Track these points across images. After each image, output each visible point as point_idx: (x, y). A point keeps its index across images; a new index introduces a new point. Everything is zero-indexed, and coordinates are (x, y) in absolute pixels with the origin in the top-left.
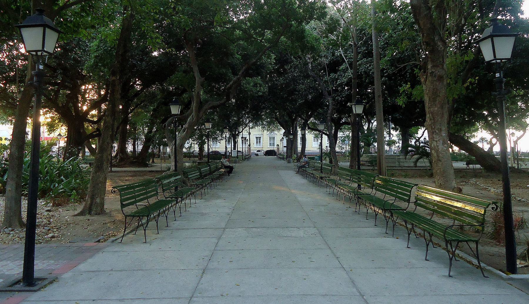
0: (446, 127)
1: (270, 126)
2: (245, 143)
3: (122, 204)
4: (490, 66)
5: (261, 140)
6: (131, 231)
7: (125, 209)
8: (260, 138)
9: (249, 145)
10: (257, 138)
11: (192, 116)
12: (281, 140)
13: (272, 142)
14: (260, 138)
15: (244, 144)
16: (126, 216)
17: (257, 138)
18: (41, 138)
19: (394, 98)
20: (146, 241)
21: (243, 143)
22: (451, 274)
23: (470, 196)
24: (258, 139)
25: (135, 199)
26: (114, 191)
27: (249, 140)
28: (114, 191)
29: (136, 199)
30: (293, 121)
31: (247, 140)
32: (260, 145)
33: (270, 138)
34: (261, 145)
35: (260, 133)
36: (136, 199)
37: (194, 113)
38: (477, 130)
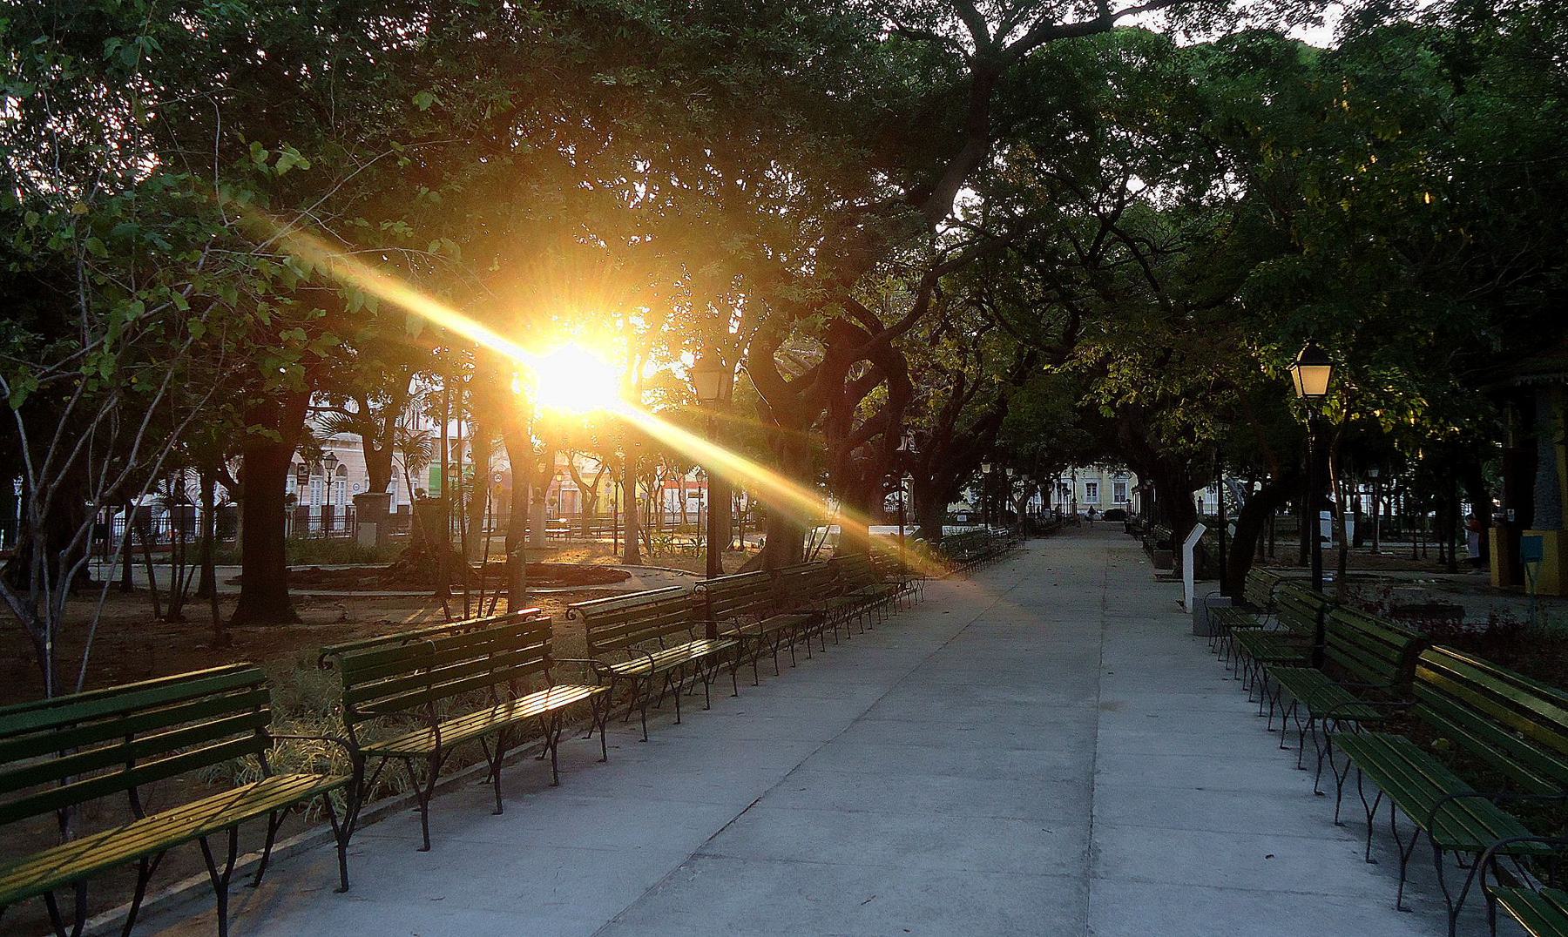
0: (309, 238)
5: (1097, 489)
8: (1096, 485)
9: (1074, 500)
10: (1088, 485)
14: (1096, 485)
17: (1088, 485)
19: (1335, 188)
20: (679, 719)
23: (1442, 653)
24: (1091, 487)
26: (572, 615)
28: (572, 615)
29: (434, 687)
30: (5, 400)
32: (1095, 500)
34: (1098, 499)
35: (1096, 475)
36: (434, 687)
38: (299, 281)
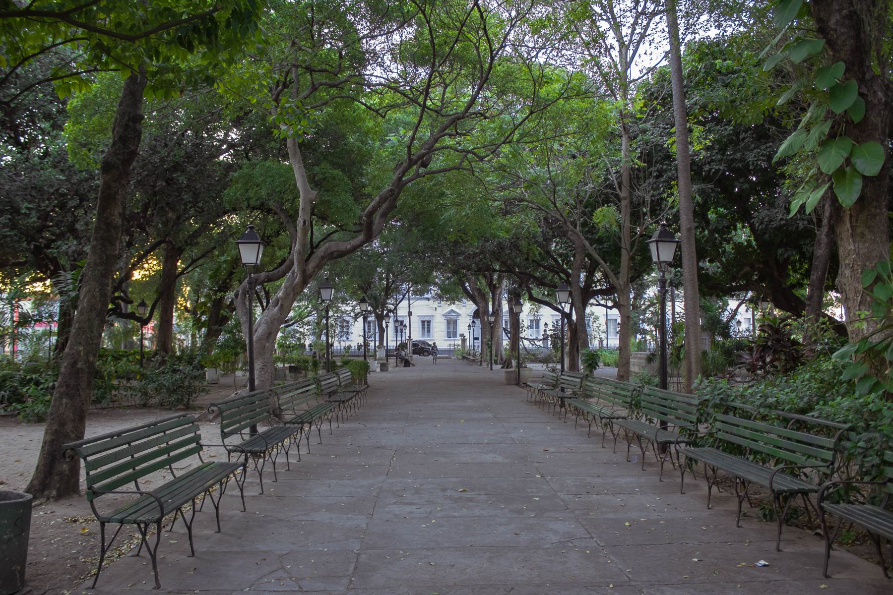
1: (448, 294)
2: (402, 332)
3: (222, 432)
4: (735, 258)
6: (563, 328)
7: (227, 441)
11: (293, 273)
12: (469, 325)
13: (452, 330)
15: (399, 334)
16: (229, 452)
18: (521, 321)
21: (396, 331)
22: (740, 524)
25: (133, 457)
27: (408, 325)
31: (405, 326)
32: (429, 336)
33: (448, 323)
37: (295, 267)
